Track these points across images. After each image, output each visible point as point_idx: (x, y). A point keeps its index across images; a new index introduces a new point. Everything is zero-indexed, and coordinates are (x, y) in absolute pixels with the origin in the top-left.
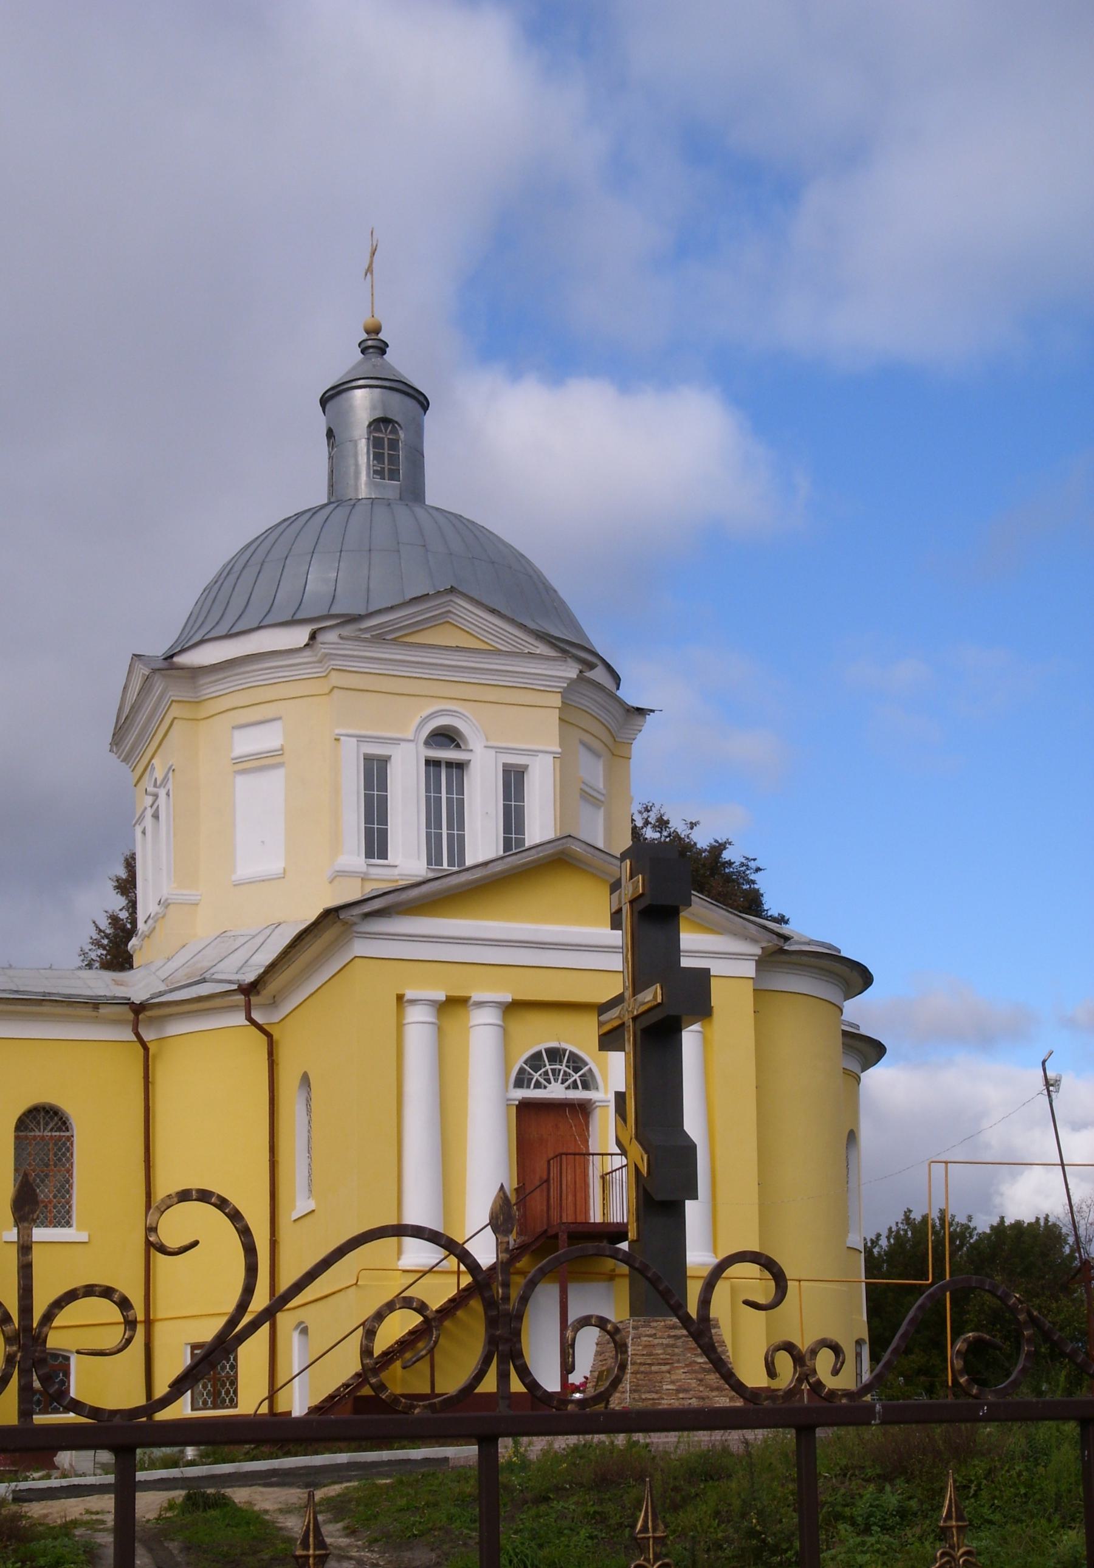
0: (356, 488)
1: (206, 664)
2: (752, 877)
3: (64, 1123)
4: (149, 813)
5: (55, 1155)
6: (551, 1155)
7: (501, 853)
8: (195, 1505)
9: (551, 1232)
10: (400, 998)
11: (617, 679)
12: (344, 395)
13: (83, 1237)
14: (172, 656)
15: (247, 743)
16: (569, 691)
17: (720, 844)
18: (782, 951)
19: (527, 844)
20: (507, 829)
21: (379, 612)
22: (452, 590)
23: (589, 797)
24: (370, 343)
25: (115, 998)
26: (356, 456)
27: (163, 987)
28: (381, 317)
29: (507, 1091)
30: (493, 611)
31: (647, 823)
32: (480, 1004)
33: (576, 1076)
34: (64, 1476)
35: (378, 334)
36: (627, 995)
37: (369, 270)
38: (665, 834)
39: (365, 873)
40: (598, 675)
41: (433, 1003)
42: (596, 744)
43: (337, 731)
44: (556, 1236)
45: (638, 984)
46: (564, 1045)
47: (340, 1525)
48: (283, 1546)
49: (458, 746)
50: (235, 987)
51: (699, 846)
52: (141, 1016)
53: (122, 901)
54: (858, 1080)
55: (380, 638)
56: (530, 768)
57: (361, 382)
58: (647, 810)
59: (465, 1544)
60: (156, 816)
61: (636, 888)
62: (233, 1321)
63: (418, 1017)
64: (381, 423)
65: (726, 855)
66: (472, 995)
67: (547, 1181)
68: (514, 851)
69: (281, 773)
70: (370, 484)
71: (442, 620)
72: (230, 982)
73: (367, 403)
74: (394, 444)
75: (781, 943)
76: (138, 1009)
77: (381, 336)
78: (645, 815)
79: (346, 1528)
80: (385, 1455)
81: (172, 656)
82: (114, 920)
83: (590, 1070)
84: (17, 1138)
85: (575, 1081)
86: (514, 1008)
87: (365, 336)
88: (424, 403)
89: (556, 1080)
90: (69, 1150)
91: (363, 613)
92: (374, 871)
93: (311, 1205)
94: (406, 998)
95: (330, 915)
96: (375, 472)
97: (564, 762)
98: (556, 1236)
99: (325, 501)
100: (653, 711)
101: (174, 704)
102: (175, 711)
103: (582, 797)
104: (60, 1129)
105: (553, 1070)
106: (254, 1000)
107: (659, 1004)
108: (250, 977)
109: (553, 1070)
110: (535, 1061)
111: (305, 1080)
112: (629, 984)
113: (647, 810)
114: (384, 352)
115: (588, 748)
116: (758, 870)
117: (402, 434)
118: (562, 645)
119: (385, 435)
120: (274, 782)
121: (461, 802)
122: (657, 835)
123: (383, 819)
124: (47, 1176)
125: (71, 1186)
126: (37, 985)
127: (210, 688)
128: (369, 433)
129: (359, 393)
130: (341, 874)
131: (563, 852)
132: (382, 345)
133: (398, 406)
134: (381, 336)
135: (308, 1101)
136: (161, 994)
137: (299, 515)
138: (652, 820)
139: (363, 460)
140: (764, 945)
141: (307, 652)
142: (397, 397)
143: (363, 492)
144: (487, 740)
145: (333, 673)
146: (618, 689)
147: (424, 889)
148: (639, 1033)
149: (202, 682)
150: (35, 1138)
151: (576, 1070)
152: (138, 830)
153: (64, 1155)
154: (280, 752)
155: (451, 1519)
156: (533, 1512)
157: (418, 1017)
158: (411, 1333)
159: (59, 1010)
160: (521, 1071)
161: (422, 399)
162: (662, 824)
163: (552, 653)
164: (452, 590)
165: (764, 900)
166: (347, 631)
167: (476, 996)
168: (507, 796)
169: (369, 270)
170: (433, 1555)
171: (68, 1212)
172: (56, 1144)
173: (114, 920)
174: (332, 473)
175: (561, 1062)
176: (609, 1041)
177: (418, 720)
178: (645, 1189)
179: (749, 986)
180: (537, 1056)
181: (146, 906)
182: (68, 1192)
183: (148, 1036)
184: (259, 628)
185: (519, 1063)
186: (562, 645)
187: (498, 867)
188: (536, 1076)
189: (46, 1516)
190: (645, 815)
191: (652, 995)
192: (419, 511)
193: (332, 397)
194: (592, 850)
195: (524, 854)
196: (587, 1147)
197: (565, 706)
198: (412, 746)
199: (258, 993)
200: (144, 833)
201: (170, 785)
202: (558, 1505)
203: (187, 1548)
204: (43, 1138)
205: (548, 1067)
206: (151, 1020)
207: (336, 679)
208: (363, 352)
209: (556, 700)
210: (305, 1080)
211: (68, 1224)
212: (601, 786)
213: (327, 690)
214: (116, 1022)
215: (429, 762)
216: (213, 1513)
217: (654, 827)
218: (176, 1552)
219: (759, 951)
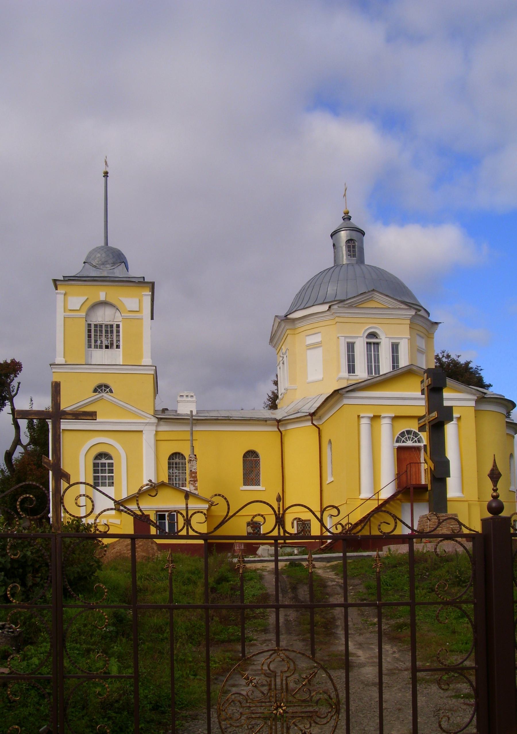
0: (343, 261)
1: (297, 317)
2: (479, 372)
3: (257, 455)
4: (281, 362)
5: (255, 465)
6: (408, 463)
7: (392, 370)
8: (292, 566)
9: (408, 487)
10: (359, 416)
11: (429, 314)
12: (338, 233)
13: (264, 489)
14: (287, 316)
15: (310, 340)
16: (412, 319)
17: (468, 362)
18: (484, 398)
19: (400, 367)
20: (393, 362)
21: (350, 299)
22: (373, 290)
23: (420, 351)
24: (345, 217)
25: (272, 418)
26: (342, 251)
27: (286, 415)
28: (349, 209)
29: (393, 443)
30: (387, 296)
31: (443, 356)
32: (384, 417)
33: (416, 439)
34: (259, 557)
35: (348, 214)
36: (427, 415)
37: (345, 195)
38: (449, 359)
39: (348, 378)
40: (422, 313)
41: (369, 417)
42: (422, 334)
43: (338, 335)
44: (409, 488)
45: (430, 411)
46: (412, 429)
47: (334, 573)
48: (315, 577)
49: (377, 338)
50: (308, 414)
51: (461, 363)
52: (280, 423)
53: (276, 387)
54: (514, 437)
55: (351, 306)
56: (400, 343)
57: (343, 229)
58: (443, 352)
59: (370, 579)
60: (283, 363)
61: (428, 383)
62: (225, 518)
63: (364, 422)
64: (349, 241)
65: (470, 365)
66: (382, 414)
67: (407, 471)
68: (396, 369)
69: (321, 348)
70: (347, 259)
71: (371, 300)
72: (307, 413)
73: (345, 235)
74: (354, 247)
75: (483, 395)
76: (279, 421)
77: (349, 214)
78: (443, 354)
79: (335, 573)
80: (355, 554)
81: (287, 316)
82: (273, 393)
83: (421, 437)
84: (243, 460)
85: (416, 440)
86: (395, 418)
87: (344, 215)
88: (363, 233)
89: (409, 440)
90: (259, 463)
91: (345, 299)
92: (351, 377)
93: (332, 479)
94: (361, 416)
95: (336, 392)
96: (348, 255)
97: (411, 341)
98: (409, 488)
99: (333, 266)
100: (441, 323)
101: (288, 330)
102: (288, 332)
103: (418, 351)
104: (256, 457)
105: (408, 437)
106: (314, 418)
107: (436, 418)
108: (312, 411)
109: (408, 437)
110: (402, 434)
111: (330, 442)
112: (427, 411)
113: (443, 352)
114: (350, 219)
115: (420, 336)
116: (481, 370)
117: (356, 244)
118: (409, 304)
119: (351, 244)
120: (318, 353)
121: (378, 355)
122: (447, 360)
123: (353, 361)
124: (252, 471)
125: (260, 474)
126: (248, 414)
127: (298, 324)
128: (346, 244)
129: (342, 232)
130: (340, 379)
131: (410, 370)
132: (349, 217)
133: (355, 235)
134: (349, 214)
135: (331, 448)
136: (285, 417)
137: (325, 271)
138: (445, 355)
139: (344, 252)
140: (478, 396)
141: (328, 312)
142: (354, 233)
143: (345, 262)
144: (386, 335)
145: (337, 318)
146: (429, 316)
147: (365, 383)
148: (430, 426)
149: (296, 323)
150: (249, 460)
151: (416, 437)
152: (278, 367)
153: (257, 465)
154: (321, 342)
155: (366, 571)
156: (391, 570)
157: (364, 422)
158: (364, 518)
159: (255, 422)
160: (398, 437)
161: (363, 232)
162: (448, 356)
163: (407, 307)
164: (373, 290)
165: (484, 379)
166: (340, 305)
167: (383, 415)
168: (393, 352)
169: (345, 195)
170: (360, 581)
171: (259, 481)
172: (255, 462)
173: (273, 393)
174: (335, 257)
175: (411, 434)
176: (422, 429)
177: (364, 330)
178: (433, 475)
179: (473, 409)
180: (403, 433)
181: (281, 391)
182: (259, 475)
183: (282, 429)
184: (313, 306)
185: (397, 435)
186: (409, 304)
187: (389, 375)
188: (403, 439)
189: (251, 567)
190: (443, 354)
191: (435, 414)
192: (362, 267)
193: (334, 234)
194: (419, 368)
195: (399, 370)
196: (420, 461)
197: (412, 323)
198: (362, 338)
199: (315, 416)
200: (280, 368)
201: (287, 354)
202: (399, 568)
203: (288, 577)
204: (251, 460)
205: (407, 436)
206: (283, 424)
207: (338, 320)
208: (343, 220)
209: (408, 322)
210: (330, 442)
211: (259, 485)
212: (424, 347)
213: (335, 323)
214: (272, 425)
215: (367, 343)
216: (296, 568)
217: (446, 358)
218: (285, 578)
219: (476, 398)
